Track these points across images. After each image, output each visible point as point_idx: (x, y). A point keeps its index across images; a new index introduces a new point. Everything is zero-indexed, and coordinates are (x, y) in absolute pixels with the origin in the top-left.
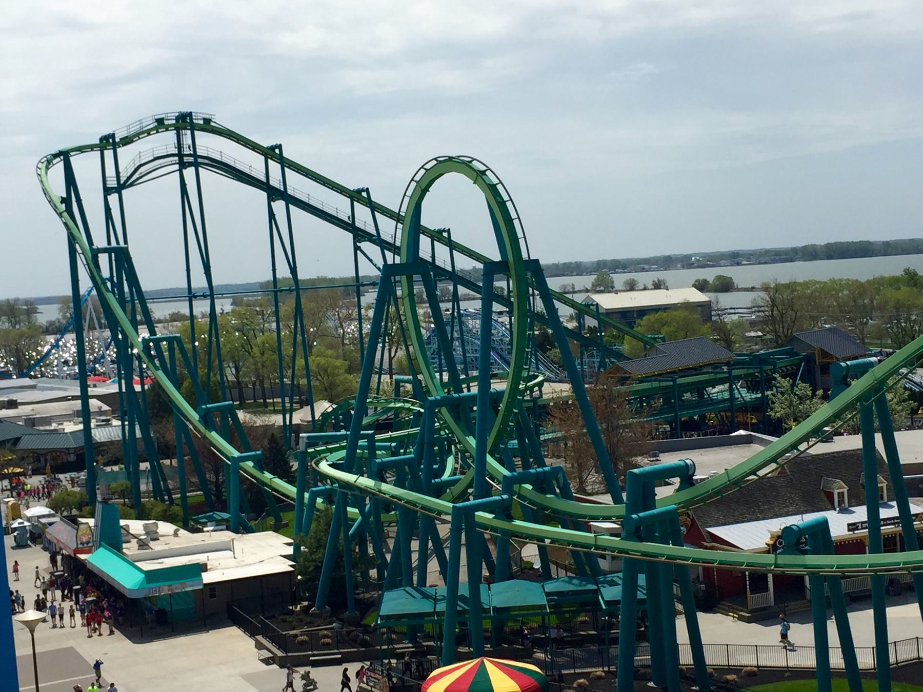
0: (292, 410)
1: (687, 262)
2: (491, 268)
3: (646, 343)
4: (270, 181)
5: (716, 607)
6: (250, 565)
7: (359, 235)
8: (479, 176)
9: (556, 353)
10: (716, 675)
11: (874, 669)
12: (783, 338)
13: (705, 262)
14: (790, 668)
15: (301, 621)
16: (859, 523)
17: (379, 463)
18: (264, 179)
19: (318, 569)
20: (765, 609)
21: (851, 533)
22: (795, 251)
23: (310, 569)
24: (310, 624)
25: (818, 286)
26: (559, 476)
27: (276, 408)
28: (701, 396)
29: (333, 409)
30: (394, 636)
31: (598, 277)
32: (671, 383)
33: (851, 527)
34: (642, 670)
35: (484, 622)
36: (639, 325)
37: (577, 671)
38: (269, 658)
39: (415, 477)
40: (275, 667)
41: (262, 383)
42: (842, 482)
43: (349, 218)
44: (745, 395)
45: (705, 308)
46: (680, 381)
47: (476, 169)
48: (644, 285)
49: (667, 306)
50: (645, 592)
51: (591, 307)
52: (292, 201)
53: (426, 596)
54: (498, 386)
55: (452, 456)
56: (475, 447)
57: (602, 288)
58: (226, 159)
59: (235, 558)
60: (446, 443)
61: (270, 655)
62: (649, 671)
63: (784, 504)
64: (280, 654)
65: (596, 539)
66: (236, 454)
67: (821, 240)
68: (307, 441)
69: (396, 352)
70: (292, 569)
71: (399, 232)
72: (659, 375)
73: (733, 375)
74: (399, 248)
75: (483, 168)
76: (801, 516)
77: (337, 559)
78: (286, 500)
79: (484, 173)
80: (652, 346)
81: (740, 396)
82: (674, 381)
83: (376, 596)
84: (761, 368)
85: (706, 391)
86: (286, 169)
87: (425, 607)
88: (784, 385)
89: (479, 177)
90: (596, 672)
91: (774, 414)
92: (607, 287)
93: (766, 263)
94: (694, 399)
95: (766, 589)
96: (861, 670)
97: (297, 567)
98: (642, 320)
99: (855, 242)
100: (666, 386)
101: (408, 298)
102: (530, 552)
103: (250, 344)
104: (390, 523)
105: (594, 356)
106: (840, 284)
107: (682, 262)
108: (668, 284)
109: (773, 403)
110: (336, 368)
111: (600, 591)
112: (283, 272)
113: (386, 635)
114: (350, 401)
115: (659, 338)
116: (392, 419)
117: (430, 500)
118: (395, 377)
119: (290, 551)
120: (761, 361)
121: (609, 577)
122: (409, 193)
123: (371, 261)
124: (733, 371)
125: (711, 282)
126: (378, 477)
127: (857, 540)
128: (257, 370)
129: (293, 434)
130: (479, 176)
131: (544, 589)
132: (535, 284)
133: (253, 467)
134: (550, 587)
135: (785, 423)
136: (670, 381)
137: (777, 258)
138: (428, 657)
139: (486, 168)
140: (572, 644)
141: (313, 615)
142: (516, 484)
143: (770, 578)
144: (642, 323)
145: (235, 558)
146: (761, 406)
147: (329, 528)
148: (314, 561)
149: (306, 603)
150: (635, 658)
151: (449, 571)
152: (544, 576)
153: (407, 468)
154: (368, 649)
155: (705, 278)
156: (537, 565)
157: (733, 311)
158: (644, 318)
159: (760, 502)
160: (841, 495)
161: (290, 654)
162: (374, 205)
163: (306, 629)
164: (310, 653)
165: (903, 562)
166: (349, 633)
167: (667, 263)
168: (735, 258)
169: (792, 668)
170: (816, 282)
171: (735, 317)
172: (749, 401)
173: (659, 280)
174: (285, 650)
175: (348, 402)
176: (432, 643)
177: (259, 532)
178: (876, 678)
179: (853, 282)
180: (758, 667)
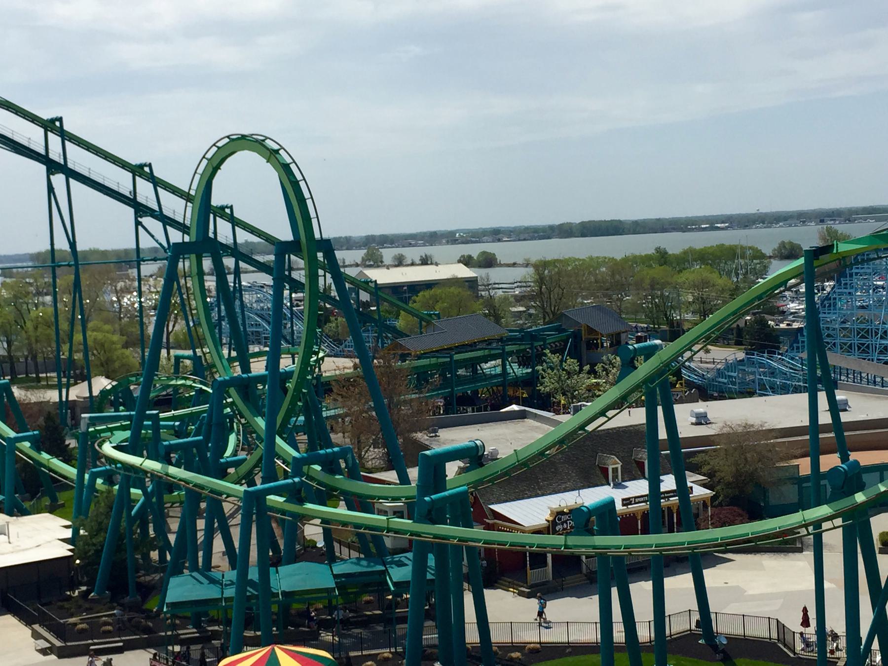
0: (68, 386)
1: (451, 238)
2: (283, 249)
3: (422, 319)
4: (218, 238)
5: (496, 583)
6: (27, 549)
7: (141, 210)
8: (272, 155)
9: (331, 327)
10: (500, 653)
11: (650, 642)
12: (551, 316)
13: (469, 239)
14: (571, 643)
15: (80, 607)
16: (632, 498)
17: (166, 446)
18: (43, 152)
19: (98, 553)
20: (544, 584)
21: (625, 507)
22: (552, 228)
23: (90, 553)
24: (89, 610)
25: (577, 263)
26: (348, 456)
27: (49, 383)
28: (475, 371)
29: (113, 386)
30: (177, 622)
31: (368, 252)
32: (449, 359)
33: (625, 502)
34: (429, 651)
35: (273, 606)
36: (415, 302)
37: (365, 653)
38: (46, 648)
39: (203, 458)
40: (53, 657)
41: (34, 358)
42: (616, 459)
43: (130, 192)
44: (516, 370)
45: (471, 283)
46: (457, 357)
47: (270, 148)
48: (412, 260)
49: (438, 282)
50: (433, 572)
51: (370, 284)
52: (71, 174)
53: (213, 581)
54: (286, 363)
55: (234, 434)
56: (264, 428)
57: (372, 263)
58: (122, 190)
59: (10, 543)
60: (228, 420)
61: (48, 645)
62: (436, 651)
63: (562, 480)
64: (58, 643)
65: (388, 522)
66: (12, 434)
67: (577, 217)
68: (89, 422)
69: (174, 326)
70: (70, 554)
71: (189, 210)
72: (437, 351)
73: (506, 350)
74: (188, 228)
75: (276, 147)
76: (577, 491)
77: (119, 540)
78: (62, 479)
79: (277, 151)
80: (429, 323)
81: (512, 371)
82: (451, 357)
83: (157, 578)
84: (532, 344)
85: (480, 367)
86: (67, 143)
87: (210, 592)
88: (554, 360)
89: (272, 156)
90: (384, 653)
91: (543, 389)
92: (377, 262)
93: (525, 240)
94: (468, 374)
95: (545, 564)
96: (641, 643)
97: (76, 551)
98: (417, 296)
99: (608, 221)
100: (444, 362)
101: (197, 277)
102: (313, 532)
103: (24, 320)
104: (173, 503)
105: (369, 331)
106: (597, 262)
107: (447, 237)
108: (435, 260)
109: (543, 378)
110: (114, 343)
111: (388, 572)
112: (62, 244)
113: (169, 621)
114: (130, 378)
115: (434, 314)
116: (171, 395)
117: (217, 483)
118: (172, 352)
119: (68, 533)
120: (533, 337)
121: (397, 558)
122: (200, 171)
123: (153, 236)
124: (506, 347)
125: (475, 258)
126: (166, 460)
127: (630, 515)
128: (30, 344)
129: (69, 411)
130: (272, 155)
131: (332, 571)
132: (327, 267)
133: (30, 447)
134: (339, 569)
135: (553, 397)
136: (447, 357)
137: (536, 235)
138: (213, 642)
139: (279, 147)
140: (357, 625)
141: (93, 600)
142: (305, 465)
143: (549, 556)
144: (417, 299)
145: (10, 543)
146: (531, 381)
147: (111, 511)
148: (94, 545)
149: (84, 588)
150: (424, 637)
151: (237, 559)
152: (328, 556)
153: (195, 450)
154: (151, 635)
155: (470, 254)
156: (321, 544)
157: (497, 286)
158: (420, 294)
159: (540, 479)
160: (615, 470)
161: (69, 644)
162: (157, 180)
163: (85, 616)
164: (90, 641)
165: (688, 542)
166: (130, 620)
167: (433, 238)
168: (496, 235)
169: (573, 643)
170: (576, 260)
171: (500, 292)
172: (520, 377)
173: (426, 256)
174: (65, 641)
175: (129, 380)
176: (216, 628)
177: (34, 514)
178: (653, 652)
179: (609, 259)
180: (540, 643)
